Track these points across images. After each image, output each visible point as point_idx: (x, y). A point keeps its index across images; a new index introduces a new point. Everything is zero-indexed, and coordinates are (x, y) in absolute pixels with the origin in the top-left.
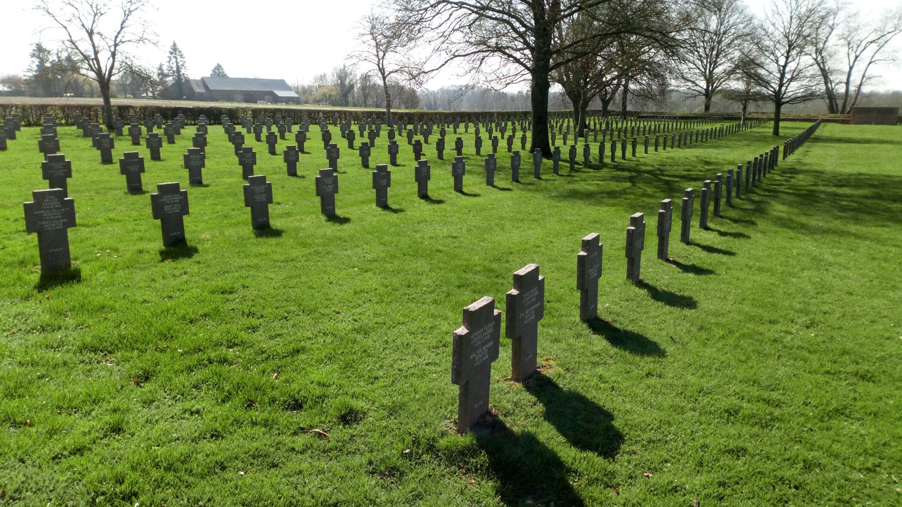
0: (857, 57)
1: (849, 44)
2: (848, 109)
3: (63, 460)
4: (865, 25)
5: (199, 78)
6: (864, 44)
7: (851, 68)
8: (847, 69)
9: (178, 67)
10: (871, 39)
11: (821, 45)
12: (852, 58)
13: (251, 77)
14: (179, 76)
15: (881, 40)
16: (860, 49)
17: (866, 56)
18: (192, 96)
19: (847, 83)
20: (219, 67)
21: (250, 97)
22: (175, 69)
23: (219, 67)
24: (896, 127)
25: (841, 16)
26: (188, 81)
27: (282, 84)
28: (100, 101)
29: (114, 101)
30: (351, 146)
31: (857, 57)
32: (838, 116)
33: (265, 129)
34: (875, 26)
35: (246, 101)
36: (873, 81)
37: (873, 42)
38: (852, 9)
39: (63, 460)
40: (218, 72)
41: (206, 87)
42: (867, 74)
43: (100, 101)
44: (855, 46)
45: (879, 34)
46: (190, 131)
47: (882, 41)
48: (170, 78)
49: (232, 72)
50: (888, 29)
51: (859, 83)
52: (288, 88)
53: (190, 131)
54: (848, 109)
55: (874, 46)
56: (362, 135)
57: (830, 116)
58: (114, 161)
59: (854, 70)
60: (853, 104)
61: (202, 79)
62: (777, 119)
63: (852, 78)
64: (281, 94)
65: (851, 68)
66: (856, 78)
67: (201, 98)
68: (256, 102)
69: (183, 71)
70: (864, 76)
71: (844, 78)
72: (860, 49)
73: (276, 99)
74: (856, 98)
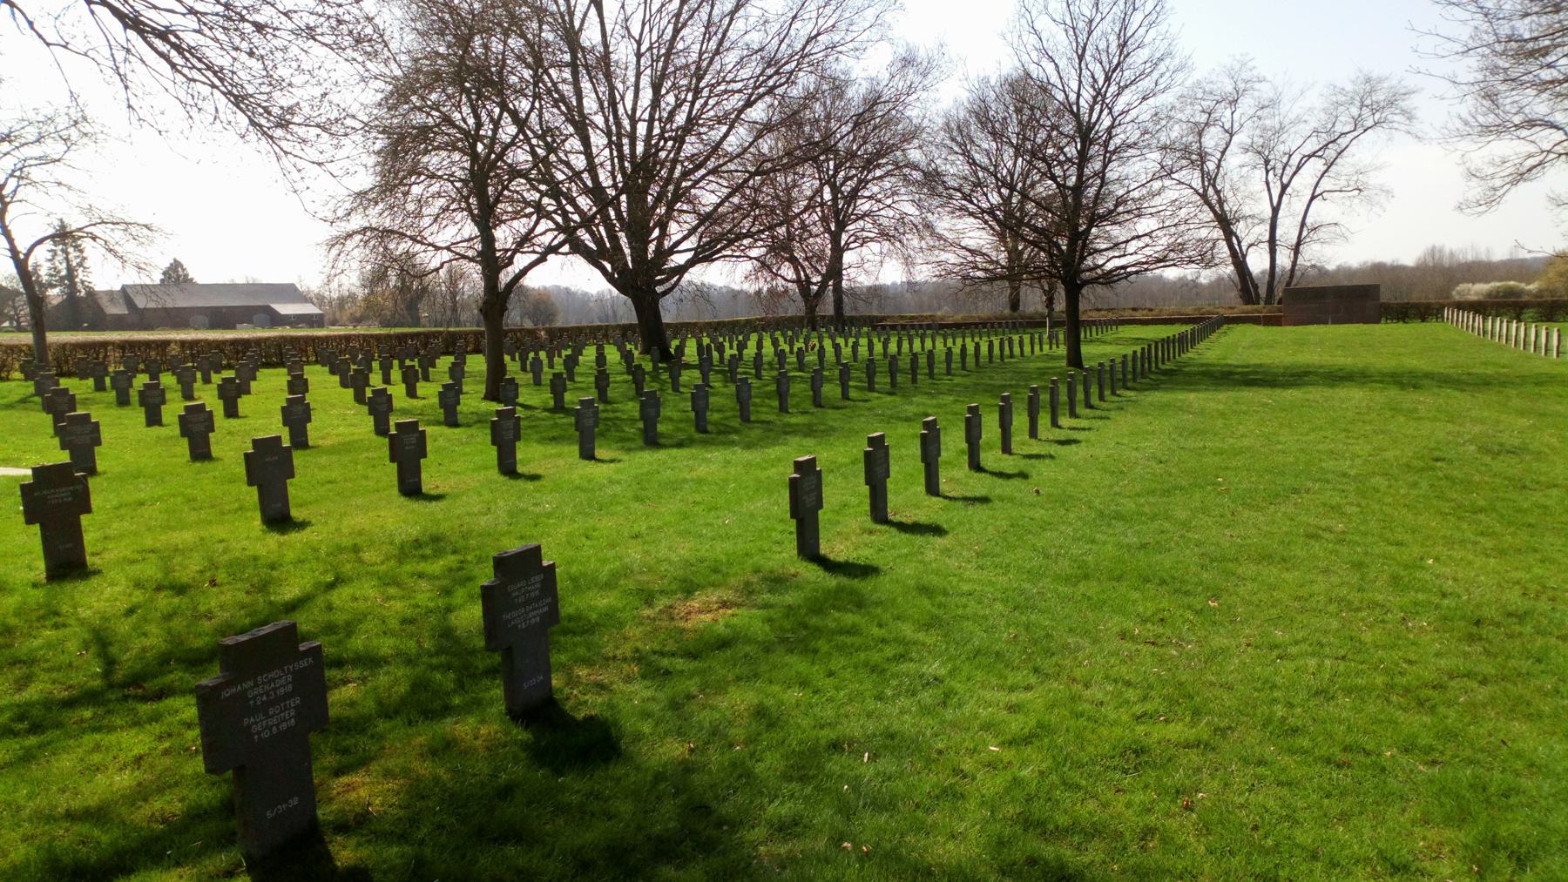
0: (1284, 188)
1: (1267, 162)
2: (1279, 293)
3: (629, 654)
4: (1298, 120)
5: (118, 288)
6: (1295, 161)
7: (1275, 210)
8: (1268, 213)
9: (70, 269)
10: (1307, 149)
11: (1211, 166)
12: (1276, 192)
13: (240, 280)
14: (73, 285)
15: (1330, 149)
16: (1289, 171)
17: (1303, 183)
18: (100, 321)
19: (1272, 242)
20: (176, 265)
21: (221, 317)
22: (64, 273)
23: (176, 265)
24: (1376, 326)
25: (1246, 105)
26: (91, 293)
27: (289, 292)
28: (27, 338)
29: (53, 337)
30: (537, 382)
31: (1284, 188)
32: (1261, 309)
33: (531, 355)
34: (1313, 124)
35: (213, 326)
36: (1321, 234)
37: (1313, 155)
38: (1265, 91)
39: (629, 654)
40: (175, 275)
41: (129, 302)
42: (1309, 221)
43: (27, 338)
44: (1279, 166)
45: (1324, 138)
46: (445, 362)
47: (1330, 153)
48: (56, 291)
49: (203, 272)
50: (1339, 128)
51: (1294, 241)
52: (303, 298)
53: (445, 362)
54: (1279, 293)
55: (1316, 165)
56: (551, 366)
57: (1242, 308)
58: (164, 420)
59: (1281, 214)
60: (1288, 284)
61: (124, 288)
62: (1074, 326)
63: (1279, 232)
64: (285, 309)
65: (1275, 210)
66: (1287, 230)
67: (119, 323)
68: (233, 328)
69: (80, 275)
70: (1303, 224)
71: (1263, 231)
72: (1289, 171)
73: (277, 320)
74: (1292, 276)
